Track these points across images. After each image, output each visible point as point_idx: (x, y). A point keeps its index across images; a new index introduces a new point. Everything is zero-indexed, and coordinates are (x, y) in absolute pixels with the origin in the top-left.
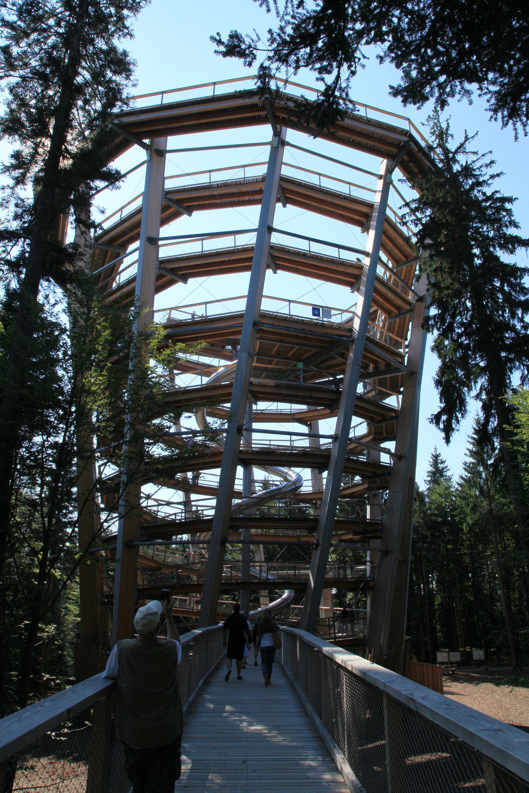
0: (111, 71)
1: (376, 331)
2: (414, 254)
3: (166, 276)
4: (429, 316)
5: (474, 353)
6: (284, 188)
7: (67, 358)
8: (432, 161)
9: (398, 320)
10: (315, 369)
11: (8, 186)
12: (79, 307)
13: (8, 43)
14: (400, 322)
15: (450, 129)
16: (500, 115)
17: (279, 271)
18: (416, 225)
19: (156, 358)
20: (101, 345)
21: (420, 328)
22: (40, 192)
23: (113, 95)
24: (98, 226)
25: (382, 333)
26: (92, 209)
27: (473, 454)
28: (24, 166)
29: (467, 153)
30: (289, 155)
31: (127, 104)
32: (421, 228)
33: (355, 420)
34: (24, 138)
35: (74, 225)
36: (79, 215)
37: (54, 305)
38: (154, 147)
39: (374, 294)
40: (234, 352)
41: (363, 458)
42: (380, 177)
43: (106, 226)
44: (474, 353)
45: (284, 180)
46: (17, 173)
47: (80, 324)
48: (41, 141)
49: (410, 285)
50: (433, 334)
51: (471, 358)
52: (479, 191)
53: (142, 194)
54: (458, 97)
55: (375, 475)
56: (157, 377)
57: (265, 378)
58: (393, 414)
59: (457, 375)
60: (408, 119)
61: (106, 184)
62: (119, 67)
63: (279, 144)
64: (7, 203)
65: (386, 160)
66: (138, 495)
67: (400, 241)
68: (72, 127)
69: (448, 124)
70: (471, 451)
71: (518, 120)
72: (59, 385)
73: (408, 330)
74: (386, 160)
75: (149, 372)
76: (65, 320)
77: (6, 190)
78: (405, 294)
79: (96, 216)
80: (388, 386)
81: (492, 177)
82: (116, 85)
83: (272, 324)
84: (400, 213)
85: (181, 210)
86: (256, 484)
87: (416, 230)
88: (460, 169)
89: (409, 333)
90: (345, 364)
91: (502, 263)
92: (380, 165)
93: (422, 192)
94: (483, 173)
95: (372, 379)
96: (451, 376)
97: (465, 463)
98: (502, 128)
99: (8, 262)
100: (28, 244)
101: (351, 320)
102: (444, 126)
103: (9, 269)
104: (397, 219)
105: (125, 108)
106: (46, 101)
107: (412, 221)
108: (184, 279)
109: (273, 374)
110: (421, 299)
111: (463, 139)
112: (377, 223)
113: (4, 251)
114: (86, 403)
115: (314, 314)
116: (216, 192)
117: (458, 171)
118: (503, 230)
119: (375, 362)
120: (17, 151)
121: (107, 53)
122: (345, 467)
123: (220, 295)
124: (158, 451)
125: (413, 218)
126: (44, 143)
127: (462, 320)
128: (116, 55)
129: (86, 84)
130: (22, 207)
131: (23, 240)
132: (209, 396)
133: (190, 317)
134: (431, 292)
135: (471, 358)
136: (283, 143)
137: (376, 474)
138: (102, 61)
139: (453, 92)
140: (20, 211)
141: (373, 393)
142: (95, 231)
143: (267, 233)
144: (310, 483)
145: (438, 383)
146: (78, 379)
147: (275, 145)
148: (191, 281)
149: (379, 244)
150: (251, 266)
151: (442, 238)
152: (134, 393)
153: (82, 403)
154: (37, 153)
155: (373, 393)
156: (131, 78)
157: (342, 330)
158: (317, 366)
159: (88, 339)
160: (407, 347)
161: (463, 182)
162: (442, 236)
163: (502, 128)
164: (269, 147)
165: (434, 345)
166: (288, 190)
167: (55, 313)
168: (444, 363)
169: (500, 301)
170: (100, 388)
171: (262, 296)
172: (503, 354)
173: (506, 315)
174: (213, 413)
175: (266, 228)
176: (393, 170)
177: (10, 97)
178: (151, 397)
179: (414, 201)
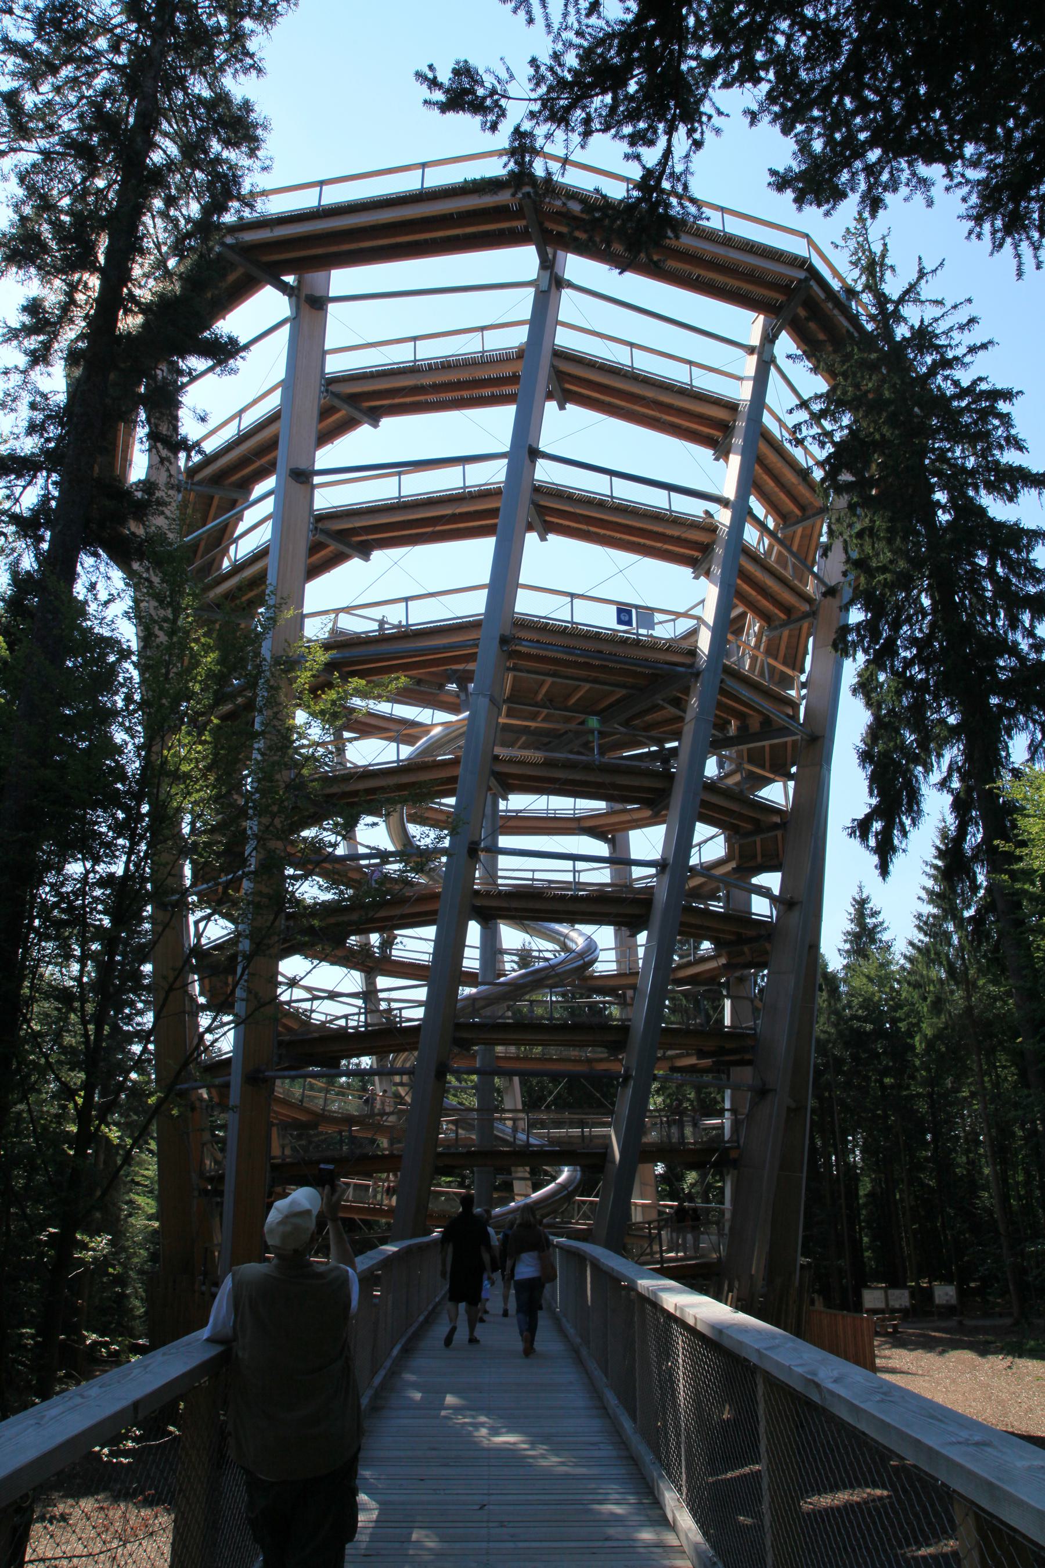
0: (219, 140)
1: (743, 655)
2: (819, 503)
3: (327, 546)
4: (847, 625)
5: (936, 698)
6: (561, 372)
7: (132, 707)
8: (854, 319)
9: (786, 633)
10: (622, 729)
11: (16, 367)
12: (155, 608)
13: (15, 84)
14: (790, 636)
15: (889, 254)
16: (987, 227)
17: (551, 537)
18: (822, 445)
19: (309, 707)
20: (200, 682)
21: (830, 648)
22: (78, 380)
23: (223, 188)
24: (193, 447)
25: (754, 659)
26: (181, 413)
27: (934, 897)
28: (48, 329)
29: (922, 302)
30: (570, 306)
31: (251, 206)
32: (832, 450)
33: (702, 831)
34: (47, 273)
35: (146, 446)
36: (157, 426)
37: (106, 603)
38: (305, 292)
39: (739, 582)
40: (463, 696)
41: (717, 907)
42: (751, 350)
43: (210, 446)
44: (936, 698)
45: (561, 355)
46: (33, 342)
47: (158, 640)
48: (80, 280)
49: (809, 563)
50: (854, 660)
51: (930, 707)
52: (946, 378)
53: (281, 384)
54: (904, 191)
55: (741, 940)
56: (309, 746)
57: (523, 747)
58: (777, 819)
59: (903, 741)
60: (806, 236)
61: (210, 363)
62: (236, 132)
63: (551, 284)
64: (14, 401)
65: (762, 317)
66: (272, 979)
67: (791, 477)
68: (142, 252)
69: (885, 245)
70: (930, 893)
71: (1023, 237)
72: (117, 762)
73: (806, 653)
74: (762, 317)
75: (295, 736)
76: (128, 633)
77: (11, 376)
78: (800, 581)
79: (189, 428)
80: (767, 764)
81: (972, 350)
82: (230, 168)
83: (538, 641)
84: (791, 421)
85: (357, 415)
86: (507, 958)
87: (822, 454)
88: (908, 335)
89: (809, 659)
90: (681, 719)
91: (991, 520)
92: (750, 325)
93: (834, 379)
94: (953, 343)
95: (734, 750)
96: (891, 744)
97: (919, 916)
98: (992, 254)
99: (16, 519)
100: (54, 483)
101: (694, 633)
102: (877, 248)
103: (17, 532)
104: (785, 433)
105: (247, 213)
106: (91, 199)
107: (814, 437)
108: (364, 551)
109: (539, 739)
110: (831, 592)
111: (915, 276)
112: (744, 441)
113: (8, 497)
114: (170, 797)
115: (620, 622)
116: (427, 381)
117: (904, 339)
118: (993, 455)
119: (741, 716)
120: (35, 299)
121: (211, 105)
122: (682, 924)
123: (434, 583)
124: (312, 891)
125: (816, 430)
126: (86, 284)
127: (913, 632)
128: (229, 109)
129: (170, 165)
130: (44, 409)
131: (45, 474)
132: (414, 784)
133: (375, 626)
134: (851, 577)
135: (930, 707)
136: (559, 283)
137: (743, 938)
138: (201, 120)
139: (895, 181)
140: (39, 417)
141: (737, 778)
142: (189, 458)
143: (527, 461)
144: (612, 955)
145: (865, 757)
146: (154, 749)
147: (544, 286)
148: (377, 555)
149: (748, 483)
150: (496, 525)
151: (873, 471)
152: (265, 778)
153: (162, 797)
154: (72, 302)
155: (737, 778)
156: (259, 153)
157: (675, 652)
158: (626, 724)
159: (175, 670)
160: (804, 685)
161: (915, 359)
162: (874, 466)
163: (992, 254)
164: (531, 291)
165: (858, 683)
166: (569, 375)
167: (109, 618)
168: (877, 717)
169: (989, 594)
170: (197, 767)
171: (518, 585)
172: (994, 700)
173: (1000, 623)
174: (421, 817)
175: (526, 450)
176: (776, 337)
177: (21, 193)
178: (298, 786)
179: (818, 397)
